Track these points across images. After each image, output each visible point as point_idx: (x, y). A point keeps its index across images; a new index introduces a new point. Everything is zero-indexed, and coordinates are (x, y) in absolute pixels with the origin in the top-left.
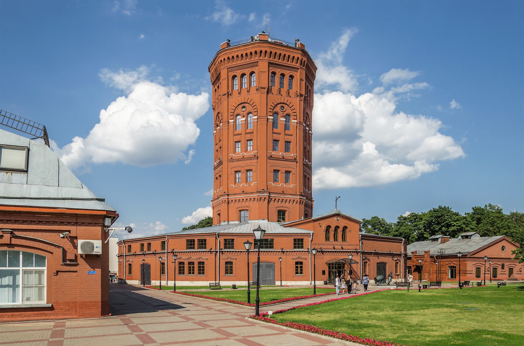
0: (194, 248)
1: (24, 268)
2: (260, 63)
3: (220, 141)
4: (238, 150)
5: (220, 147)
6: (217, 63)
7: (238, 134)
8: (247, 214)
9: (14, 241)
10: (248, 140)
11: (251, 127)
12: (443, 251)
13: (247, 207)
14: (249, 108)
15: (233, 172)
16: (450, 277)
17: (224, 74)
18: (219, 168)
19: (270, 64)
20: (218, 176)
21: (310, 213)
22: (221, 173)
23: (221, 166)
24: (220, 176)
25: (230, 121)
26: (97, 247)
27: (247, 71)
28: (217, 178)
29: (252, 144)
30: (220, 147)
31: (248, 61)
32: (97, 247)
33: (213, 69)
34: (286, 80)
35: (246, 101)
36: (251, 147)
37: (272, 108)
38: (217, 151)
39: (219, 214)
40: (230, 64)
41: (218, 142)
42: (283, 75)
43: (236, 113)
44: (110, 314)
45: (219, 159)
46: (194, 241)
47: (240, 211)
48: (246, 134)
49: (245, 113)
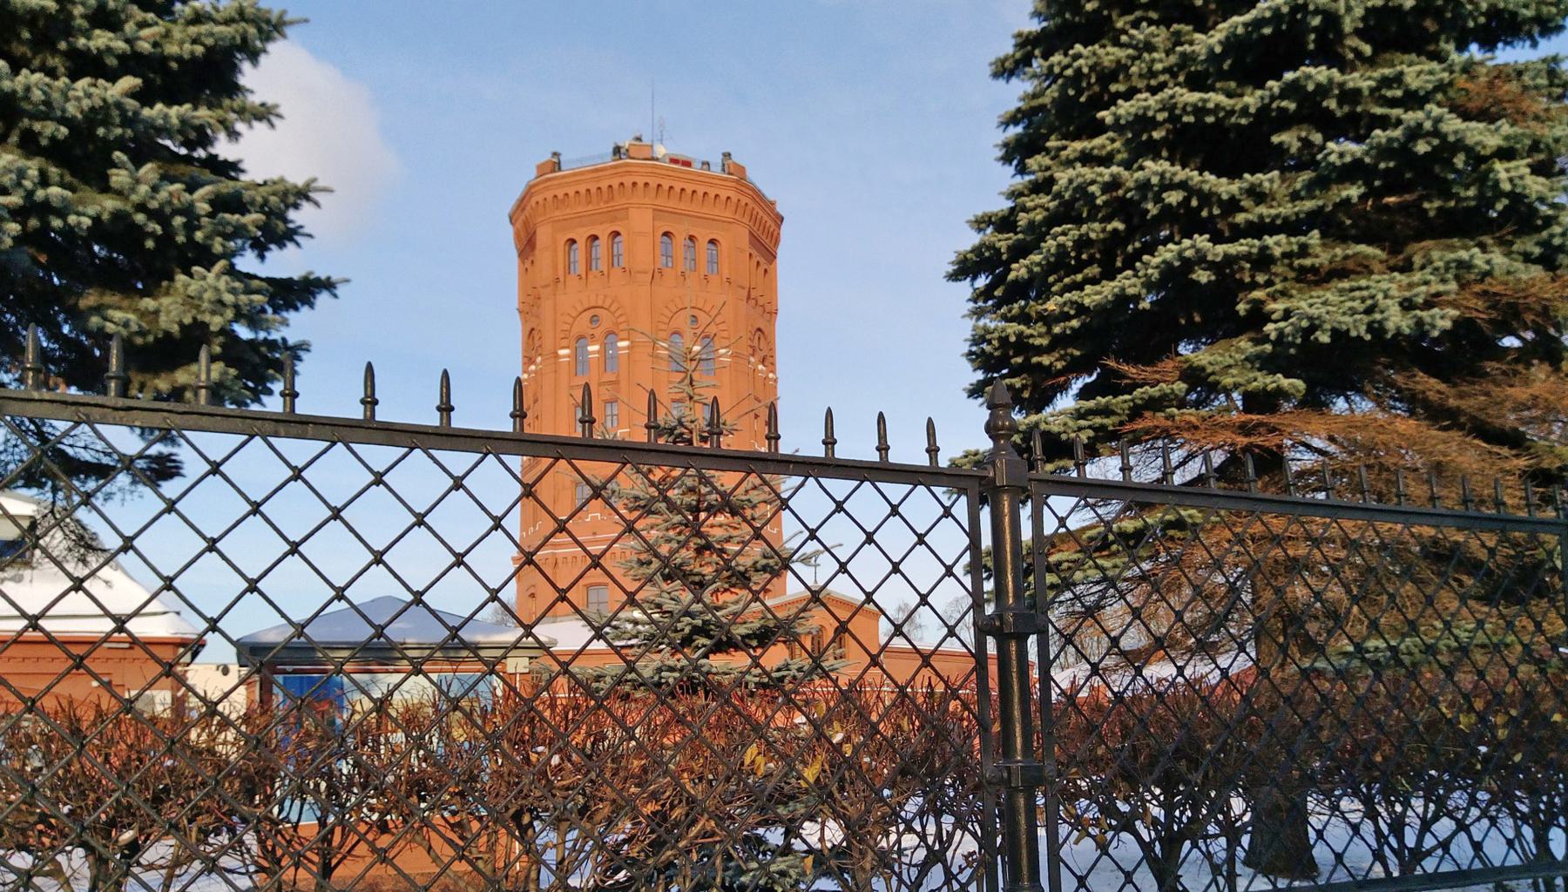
2: (633, 213)
14: (607, 321)
17: (543, 236)
25: (562, 352)
48: (600, 384)
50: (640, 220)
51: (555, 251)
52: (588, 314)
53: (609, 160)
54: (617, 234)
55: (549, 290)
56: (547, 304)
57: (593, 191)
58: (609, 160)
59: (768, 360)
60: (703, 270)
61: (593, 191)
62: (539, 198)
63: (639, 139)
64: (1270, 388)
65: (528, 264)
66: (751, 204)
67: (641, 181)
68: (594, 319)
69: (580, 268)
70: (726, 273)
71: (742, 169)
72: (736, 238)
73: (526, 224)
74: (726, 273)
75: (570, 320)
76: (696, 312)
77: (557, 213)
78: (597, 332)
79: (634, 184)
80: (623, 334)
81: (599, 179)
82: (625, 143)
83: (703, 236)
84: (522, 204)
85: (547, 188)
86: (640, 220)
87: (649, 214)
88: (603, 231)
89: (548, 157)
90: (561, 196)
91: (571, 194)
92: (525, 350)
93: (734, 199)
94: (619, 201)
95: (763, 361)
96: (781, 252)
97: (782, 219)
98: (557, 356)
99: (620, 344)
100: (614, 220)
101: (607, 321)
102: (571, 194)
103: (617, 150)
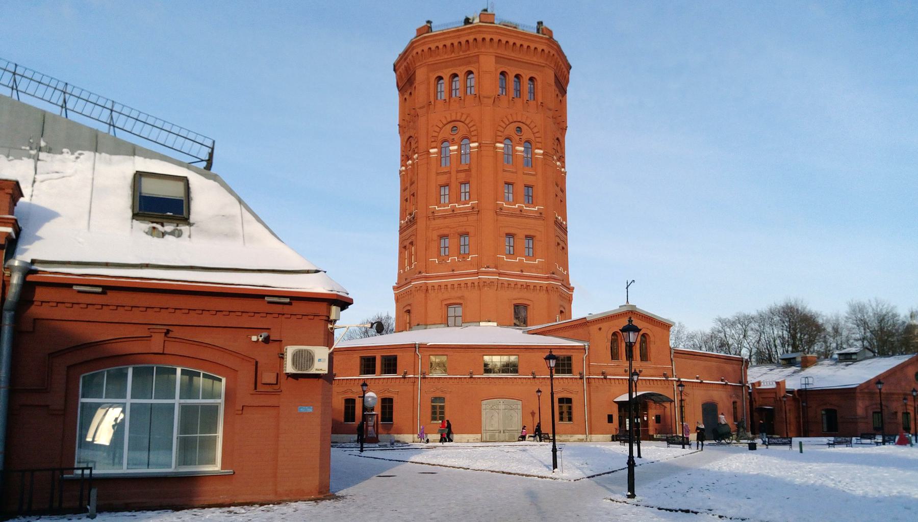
0: (374, 373)
1: (183, 401)
2: (482, 59)
3: (412, 183)
4: (445, 200)
5: (413, 195)
6: (410, 57)
7: (445, 173)
8: (459, 311)
9: (171, 348)
10: (461, 183)
11: (465, 160)
12: (810, 381)
13: (460, 298)
14: (462, 129)
15: (435, 237)
16: (825, 430)
17: (421, 74)
18: (411, 229)
19: (498, 58)
20: (407, 243)
21: (567, 311)
22: (413, 238)
23: (415, 227)
24: (412, 243)
25: (432, 151)
26: (320, 360)
27: (461, 71)
28: (405, 247)
29: (467, 190)
30: (413, 195)
31: (513, 55)
32: (320, 360)
33: (403, 67)
34: (526, 85)
35: (458, 119)
36: (447, 197)
37: (437, 129)
38: (406, 200)
39: (409, 312)
40: (431, 60)
41: (408, 185)
42: (517, 76)
43: (441, 137)
44: (879, 439)
45: (410, 214)
46: (374, 359)
47: (448, 305)
48: (458, 172)
49: (456, 138)
50: (488, 63)
51: (429, 84)
52: (449, 126)
53: (461, 25)
54: (470, 72)
55: (425, 109)
56: (422, 120)
57: (456, 44)
58: (461, 25)
59: (562, 158)
60: (526, 96)
61: (456, 44)
62: (419, 50)
63: (486, 10)
64: (817, 484)
65: (407, 96)
66: (556, 55)
67: (488, 37)
68: (454, 128)
69: (444, 96)
70: (540, 101)
71: (550, 32)
72: (546, 78)
73: (407, 69)
74: (540, 101)
75: (437, 129)
76: (520, 125)
77: (431, 59)
78: (456, 138)
79: (484, 39)
80: (475, 139)
81: (459, 36)
82: (489, 11)
83: (526, 74)
84: (404, 56)
85: (424, 44)
86: (488, 63)
87: (493, 59)
88: (461, 71)
89: (424, 23)
90: (433, 48)
91: (441, 46)
92: (402, 151)
93: (546, 51)
94: (473, 51)
95: (559, 160)
96: (569, 89)
97: (570, 67)
98: (429, 153)
99: (472, 145)
100: (469, 63)
101: (462, 129)
102: (441, 46)
103: (467, 21)
